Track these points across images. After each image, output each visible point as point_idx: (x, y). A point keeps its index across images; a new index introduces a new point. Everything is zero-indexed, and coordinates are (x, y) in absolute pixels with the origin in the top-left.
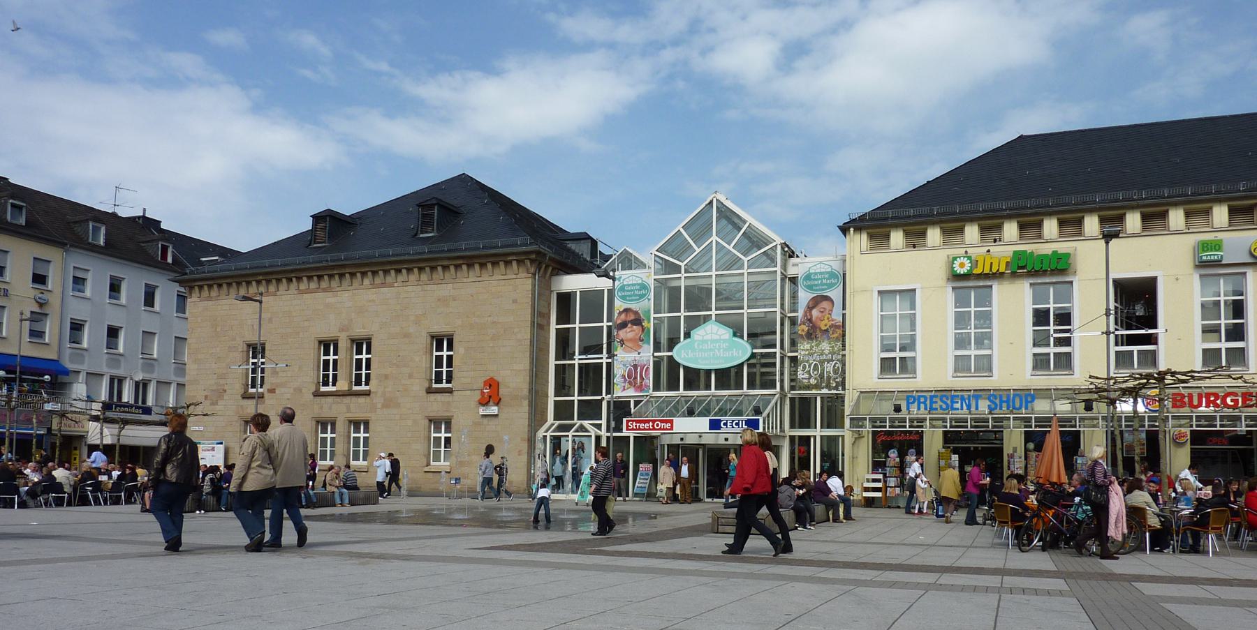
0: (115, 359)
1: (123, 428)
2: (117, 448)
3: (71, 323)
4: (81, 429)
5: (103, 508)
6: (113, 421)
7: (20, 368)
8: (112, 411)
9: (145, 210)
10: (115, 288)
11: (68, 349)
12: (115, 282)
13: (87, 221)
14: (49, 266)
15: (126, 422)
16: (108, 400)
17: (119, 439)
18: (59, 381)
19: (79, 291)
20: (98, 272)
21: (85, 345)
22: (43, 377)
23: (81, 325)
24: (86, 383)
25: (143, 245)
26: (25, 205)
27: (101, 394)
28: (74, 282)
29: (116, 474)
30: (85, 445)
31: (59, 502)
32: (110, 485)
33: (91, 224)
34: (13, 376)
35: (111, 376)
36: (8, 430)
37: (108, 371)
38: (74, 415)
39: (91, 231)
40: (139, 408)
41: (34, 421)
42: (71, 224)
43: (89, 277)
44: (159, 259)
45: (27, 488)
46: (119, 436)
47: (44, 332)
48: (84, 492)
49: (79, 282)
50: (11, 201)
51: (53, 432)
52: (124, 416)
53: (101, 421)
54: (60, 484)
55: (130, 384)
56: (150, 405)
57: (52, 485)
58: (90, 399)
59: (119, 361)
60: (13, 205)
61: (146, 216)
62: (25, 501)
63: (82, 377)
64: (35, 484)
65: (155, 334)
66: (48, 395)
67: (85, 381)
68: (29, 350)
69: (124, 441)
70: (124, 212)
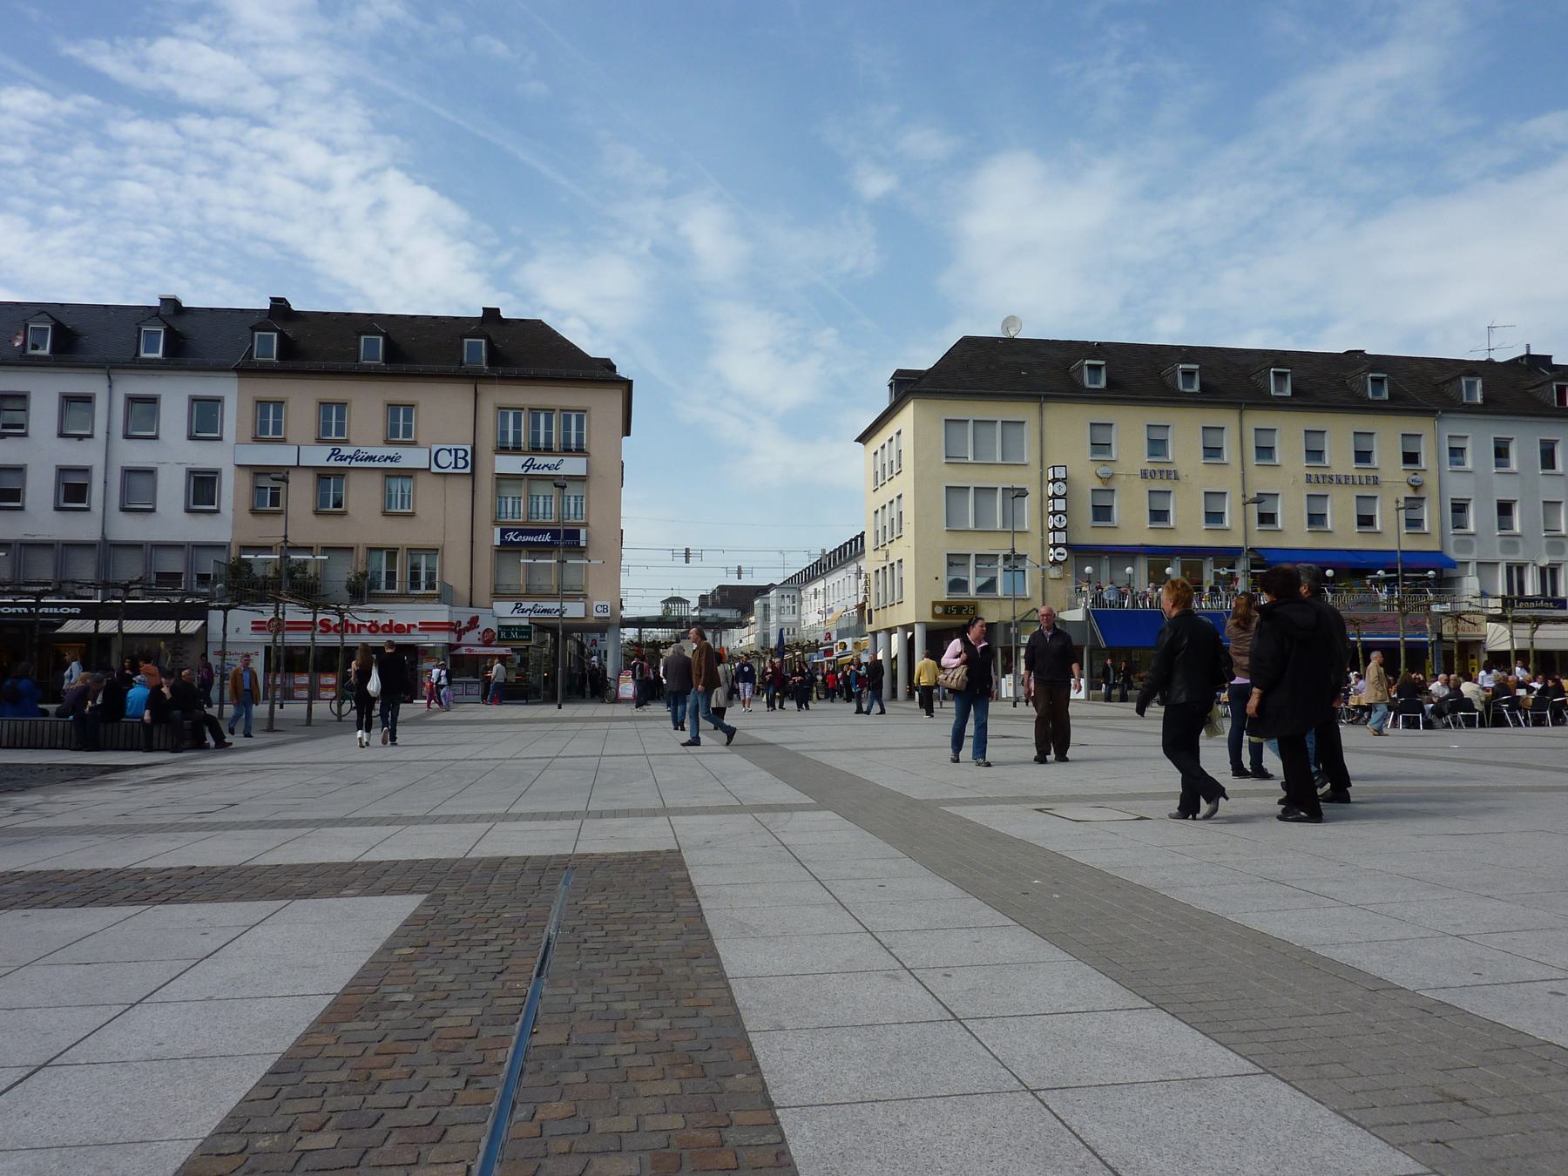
0: (1511, 542)
1: (1537, 628)
2: (1513, 655)
3: (1452, 504)
4: (1477, 633)
5: (1523, 730)
6: (1522, 620)
7: (1401, 566)
8: (1514, 607)
9: (1528, 346)
10: (1501, 452)
11: (1452, 536)
12: (1502, 446)
13: (1459, 377)
14: (1420, 441)
15: (1539, 621)
16: (1506, 594)
17: (1532, 643)
18: (1445, 576)
19: (1458, 464)
20: (1478, 437)
21: (1472, 528)
22: (1427, 573)
23: (1464, 504)
24: (1478, 575)
25: (1531, 391)
26: (1385, 375)
27: (1496, 587)
28: (1451, 455)
29: (1537, 685)
30: (1485, 652)
31: (1470, 723)
32: (1531, 701)
33: (1463, 381)
34: (1395, 575)
35: (1507, 563)
36: (1402, 638)
37: (1503, 558)
38: (1472, 616)
39: (1464, 389)
40: (1549, 601)
41: (1428, 626)
42: (1440, 386)
43: (1468, 445)
44: (1556, 405)
45: (1432, 705)
46: (1532, 638)
47: (1422, 520)
48: (1497, 710)
49: (1457, 453)
50: (1087, 362)
51: (1444, 638)
52: (1536, 612)
53: (1509, 621)
54: (1469, 700)
55: (1533, 572)
56: (1563, 596)
57: (1458, 703)
58: (1483, 595)
59: (1471, 543)
60: (1373, 380)
61: (1531, 353)
62: (1430, 720)
63: (1472, 568)
64: (1443, 700)
65: (1560, 503)
66: (1332, 593)
67: (1475, 573)
68: (1409, 544)
69: (1539, 646)
70: (1500, 357)
